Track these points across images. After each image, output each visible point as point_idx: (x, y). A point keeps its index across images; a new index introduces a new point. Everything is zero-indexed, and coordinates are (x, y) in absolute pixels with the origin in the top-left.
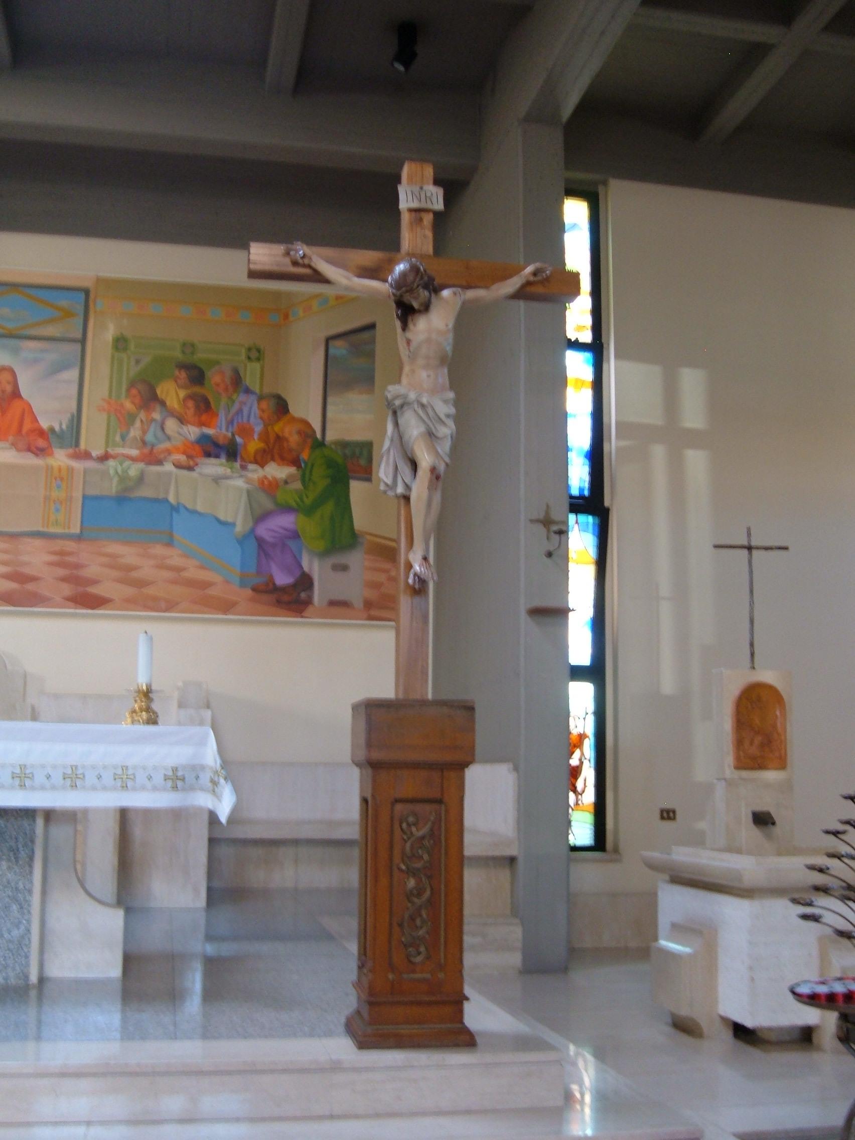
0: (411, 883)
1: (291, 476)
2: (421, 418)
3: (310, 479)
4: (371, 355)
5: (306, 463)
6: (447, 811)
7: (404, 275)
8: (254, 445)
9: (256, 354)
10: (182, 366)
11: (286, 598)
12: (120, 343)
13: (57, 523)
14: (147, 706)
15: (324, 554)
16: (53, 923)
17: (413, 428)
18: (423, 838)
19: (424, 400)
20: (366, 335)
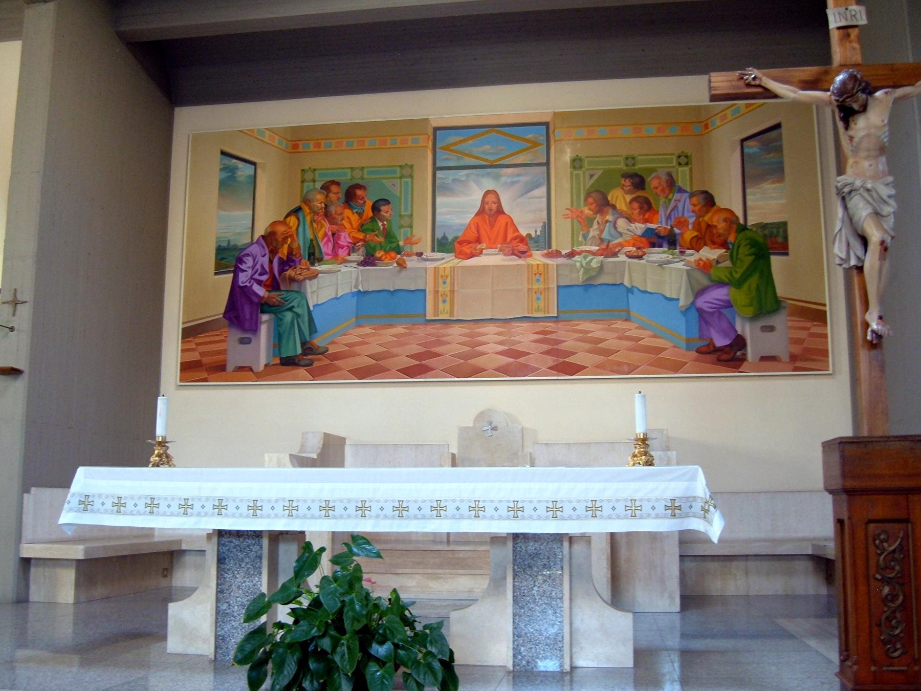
0: (886, 590)
1: (721, 256)
2: (868, 202)
3: (737, 259)
4: (779, 150)
5: (733, 245)
6: (913, 530)
7: (844, 83)
8: (689, 234)
9: (684, 159)
10: (626, 176)
11: (724, 357)
12: (576, 163)
13: (538, 309)
14: (645, 450)
15: (754, 318)
16: (577, 623)
17: (862, 210)
18: (894, 551)
19: (869, 186)
20: (774, 134)
